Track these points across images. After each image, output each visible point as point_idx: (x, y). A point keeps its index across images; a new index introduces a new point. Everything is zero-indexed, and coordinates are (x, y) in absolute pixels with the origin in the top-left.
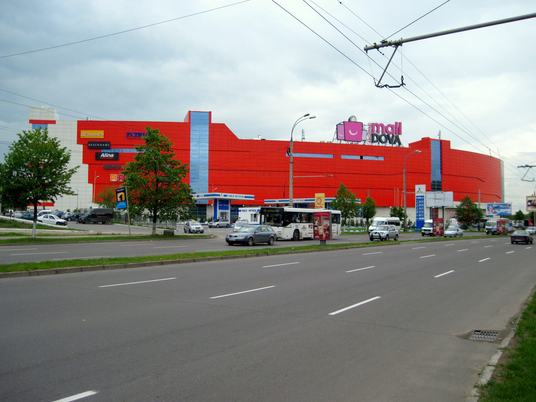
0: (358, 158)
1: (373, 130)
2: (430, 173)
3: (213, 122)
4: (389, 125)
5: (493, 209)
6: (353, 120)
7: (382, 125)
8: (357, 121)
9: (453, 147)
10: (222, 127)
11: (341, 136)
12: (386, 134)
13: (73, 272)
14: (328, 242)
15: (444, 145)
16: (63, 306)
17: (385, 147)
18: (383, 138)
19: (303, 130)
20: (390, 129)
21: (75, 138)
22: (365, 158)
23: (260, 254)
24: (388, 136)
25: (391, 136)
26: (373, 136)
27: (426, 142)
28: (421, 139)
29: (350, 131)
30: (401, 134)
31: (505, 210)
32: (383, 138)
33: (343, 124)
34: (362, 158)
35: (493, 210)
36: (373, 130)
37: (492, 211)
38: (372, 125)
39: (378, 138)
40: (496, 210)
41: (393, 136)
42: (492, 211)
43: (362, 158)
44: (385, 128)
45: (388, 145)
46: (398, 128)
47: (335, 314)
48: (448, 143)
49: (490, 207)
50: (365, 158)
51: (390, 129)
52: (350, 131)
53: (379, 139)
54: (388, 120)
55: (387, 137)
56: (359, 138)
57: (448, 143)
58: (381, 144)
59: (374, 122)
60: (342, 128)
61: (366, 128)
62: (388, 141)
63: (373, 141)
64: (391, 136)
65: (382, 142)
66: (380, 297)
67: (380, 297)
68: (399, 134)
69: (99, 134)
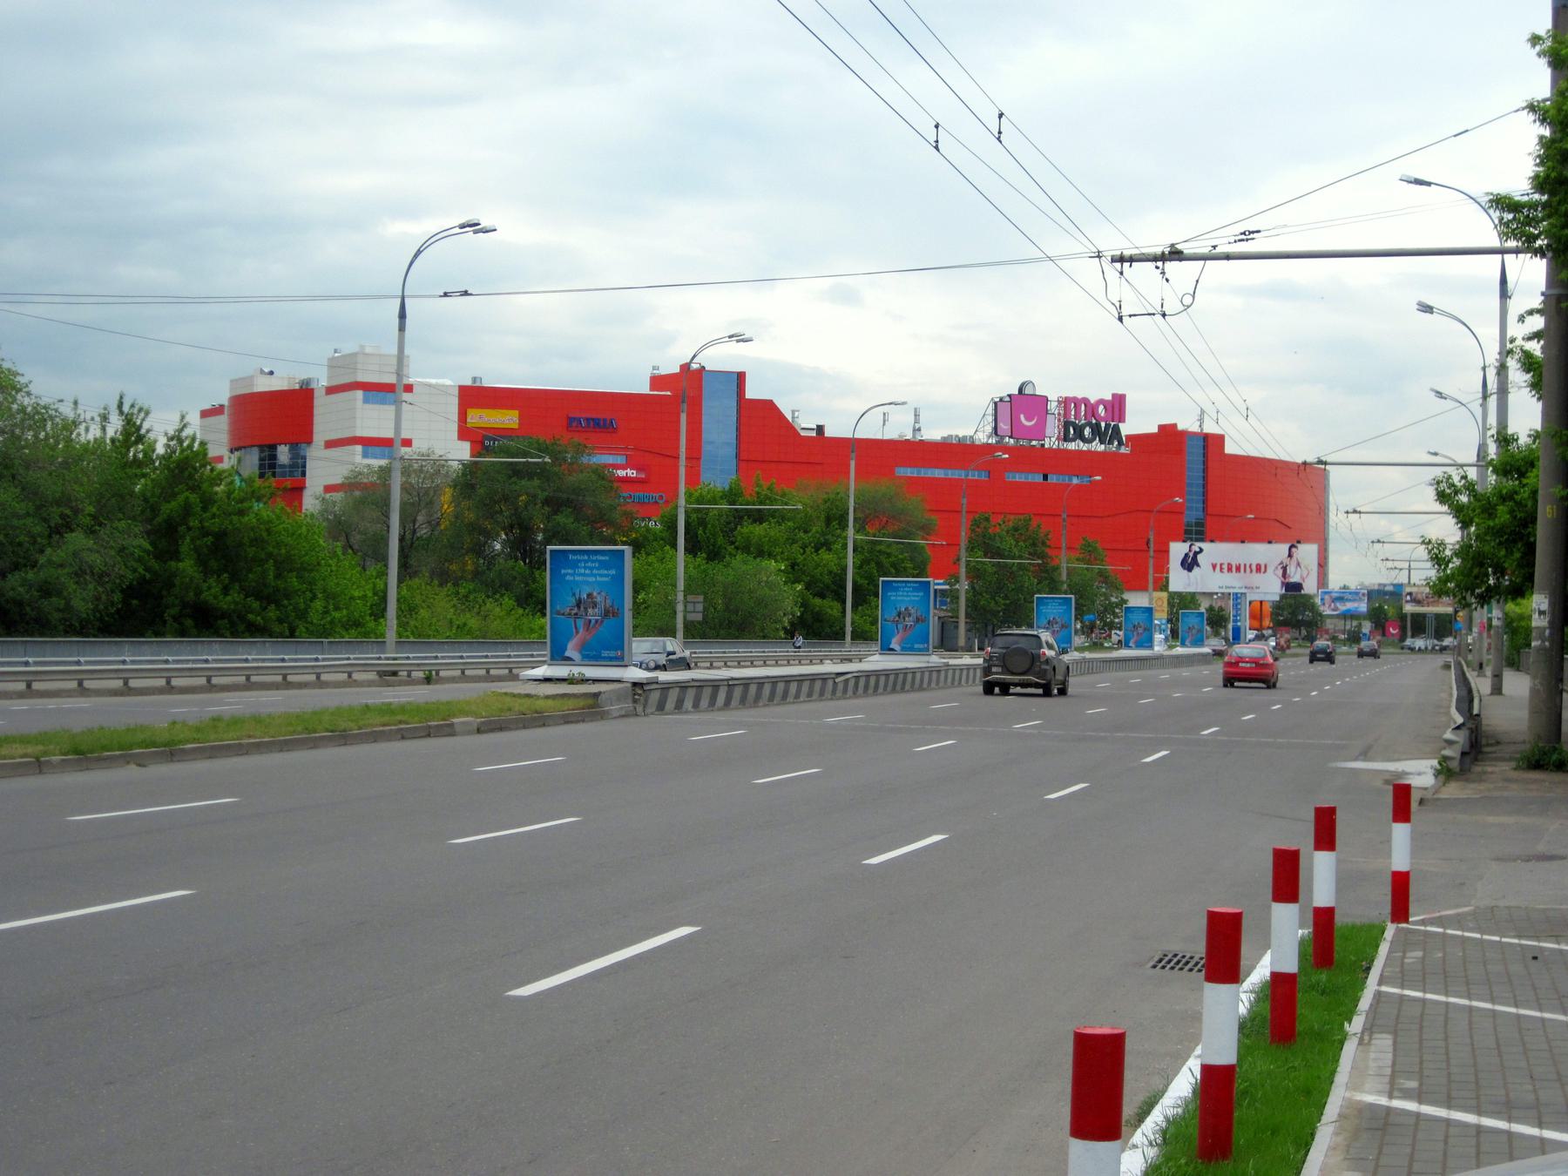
0: (1038, 478)
1: (1067, 409)
2: (1182, 513)
3: (750, 394)
4: (1101, 401)
5: (1333, 602)
6: (1028, 391)
7: (1086, 401)
8: (1037, 393)
9: (1230, 448)
10: (768, 407)
11: (1004, 427)
12: (1094, 421)
13: (20, 776)
14: (1288, 652)
15: (1211, 443)
16: (1348, 679)
17: (1089, 452)
18: (1087, 431)
19: (916, 409)
20: (1101, 410)
21: (454, 427)
22: (1038, 478)
23: (183, 751)
24: (1098, 425)
25: (1103, 424)
26: (1067, 425)
27: (1169, 433)
28: (1155, 430)
29: (1022, 417)
30: (1124, 421)
31: (1356, 605)
32: (1087, 431)
33: (1008, 399)
34: (1045, 477)
35: (1333, 604)
36: (1066, 414)
37: (1330, 606)
38: (1065, 402)
39: (1078, 431)
40: (1338, 605)
41: (1107, 426)
42: (1330, 606)
43: (1045, 477)
44: (1092, 409)
45: (1096, 446)
46: (1117, 405)
47: (607, 964)
48: (1220, 439)
49: (1327, 597)
50: (1053, 479)
51: (1101, 410)
52: (1022, 417)
53: (1079, 435)
54: (1098, 391)
55: (1096, 430)
56: (1040, 432)
57: (1220, 439)
58: (1085, 447)
59: (1071, 394)
60: (1005, 410)
61: (1052, 406)
62: (1098, 439)
63: (1066, 439)
64: (1103, 424)
65: (1085, 440)
66: (864, 862)
67: (864, 862)
68: (1120, 422)
69: (508, 419)
